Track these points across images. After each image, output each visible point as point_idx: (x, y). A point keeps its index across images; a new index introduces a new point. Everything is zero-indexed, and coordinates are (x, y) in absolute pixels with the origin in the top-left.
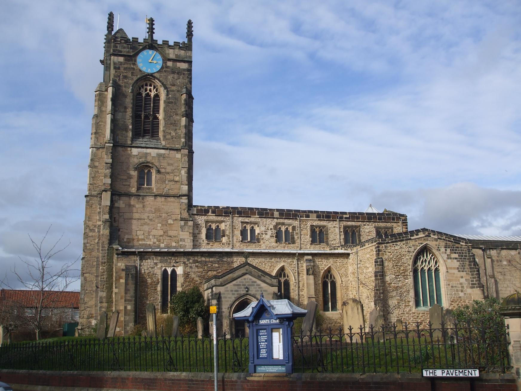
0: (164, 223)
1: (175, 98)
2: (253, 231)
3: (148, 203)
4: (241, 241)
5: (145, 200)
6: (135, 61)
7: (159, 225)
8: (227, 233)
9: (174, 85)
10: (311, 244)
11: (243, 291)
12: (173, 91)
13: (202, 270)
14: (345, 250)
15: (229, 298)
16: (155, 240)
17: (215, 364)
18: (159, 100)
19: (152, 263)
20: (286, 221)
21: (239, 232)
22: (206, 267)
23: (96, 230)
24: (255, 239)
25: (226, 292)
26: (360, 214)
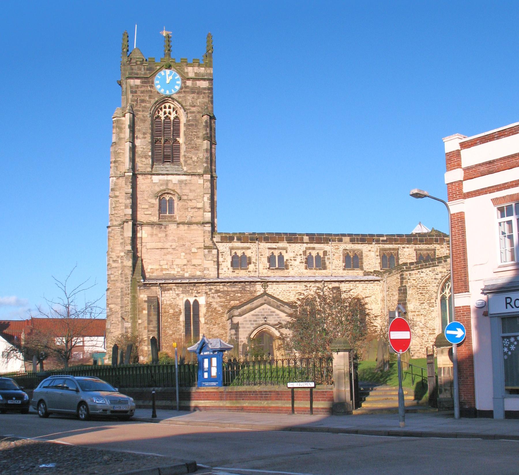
0: (188, 251)
1: (196, 120)
2: (281, 257)
3: (171, 231)
4: (269, 268)
5: (167, 229)
6: (153, 83)
7: (183, 254)
8: (253, 260)
9: (194, 106)
10: (344, 269)
11: (261, 321)
12: (193, 112)
13: (224, 300)
14: (377, 276)
15: (248, 328)
16: (179, 270)
17: (177, 378)
18: (179, 123)
19: (175, 295)
20: (316, 246)
21: (266, 259)
22: (228, 297)
23: (120, 261)
24: (283, 265)
25: (244, 323)
26: (399, 235)
